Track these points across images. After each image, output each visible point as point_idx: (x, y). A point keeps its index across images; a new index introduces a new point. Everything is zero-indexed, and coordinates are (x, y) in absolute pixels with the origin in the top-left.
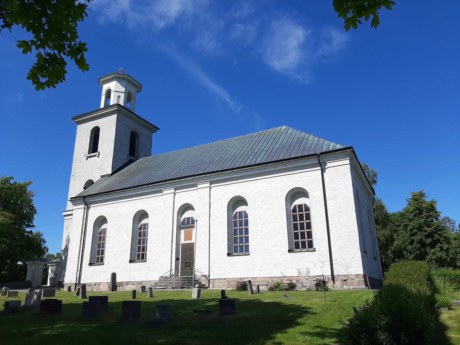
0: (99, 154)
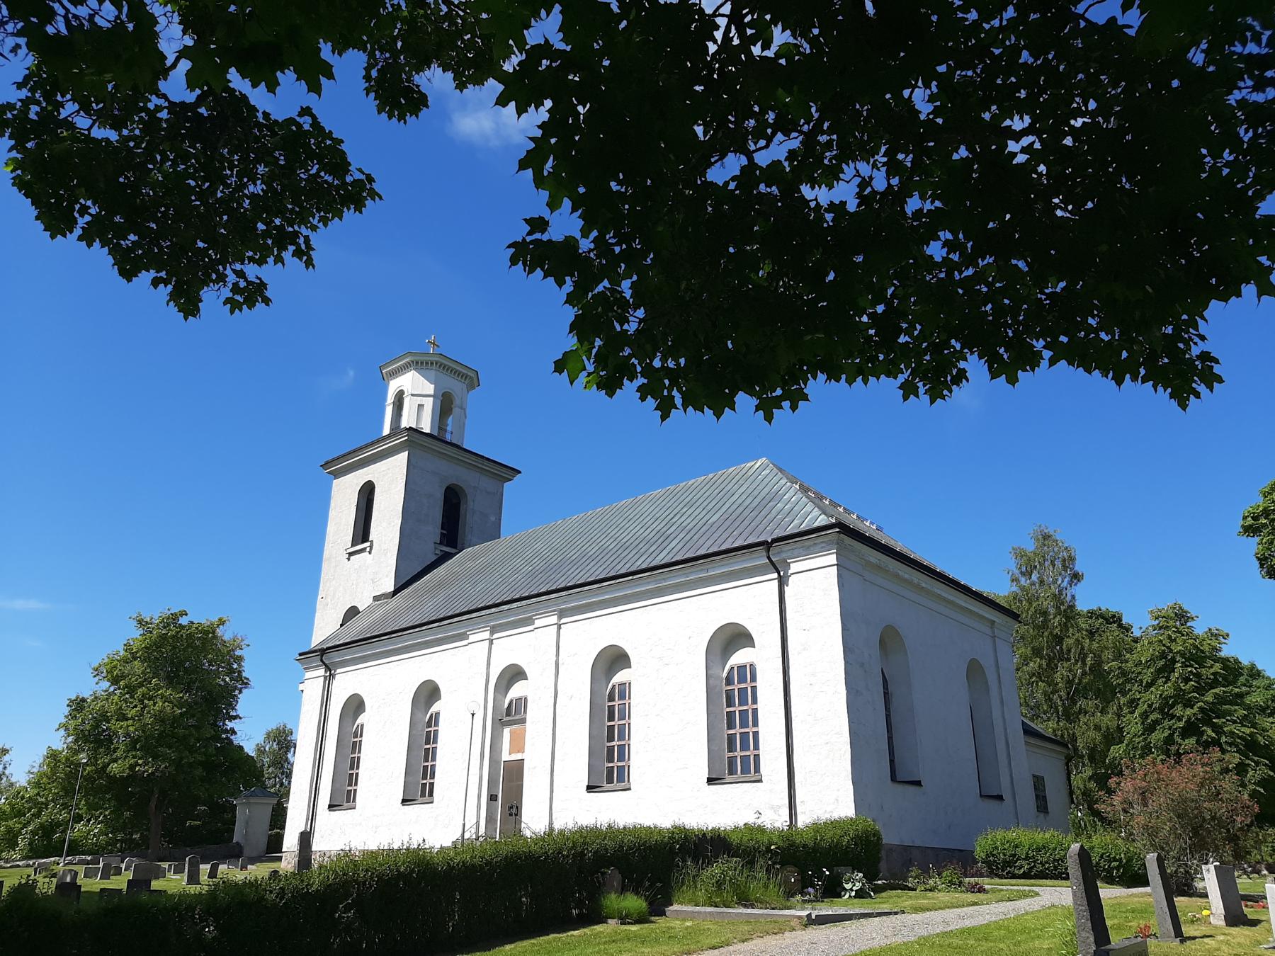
0: (371, 547)
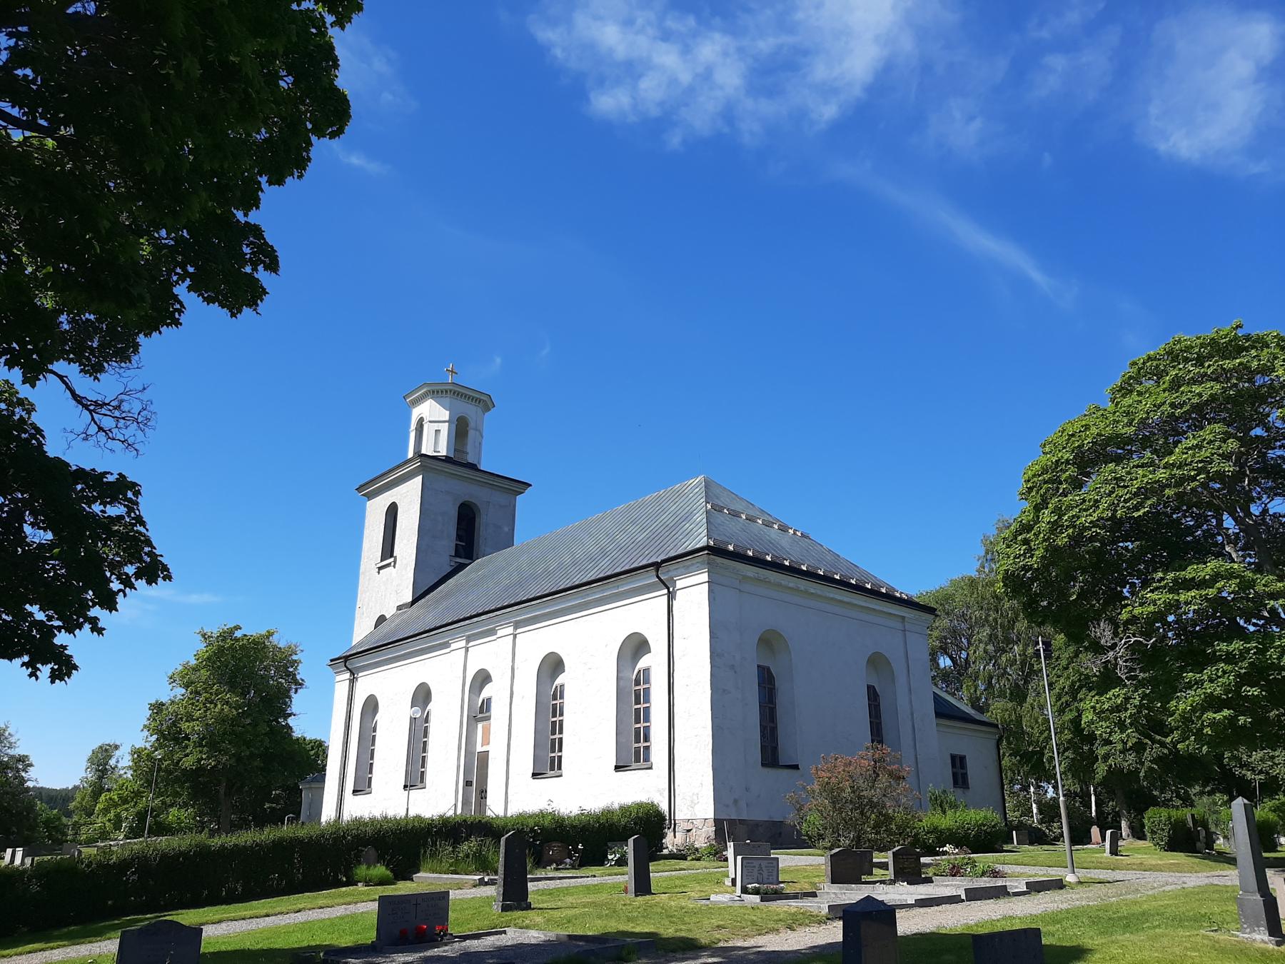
0: (395, 562)
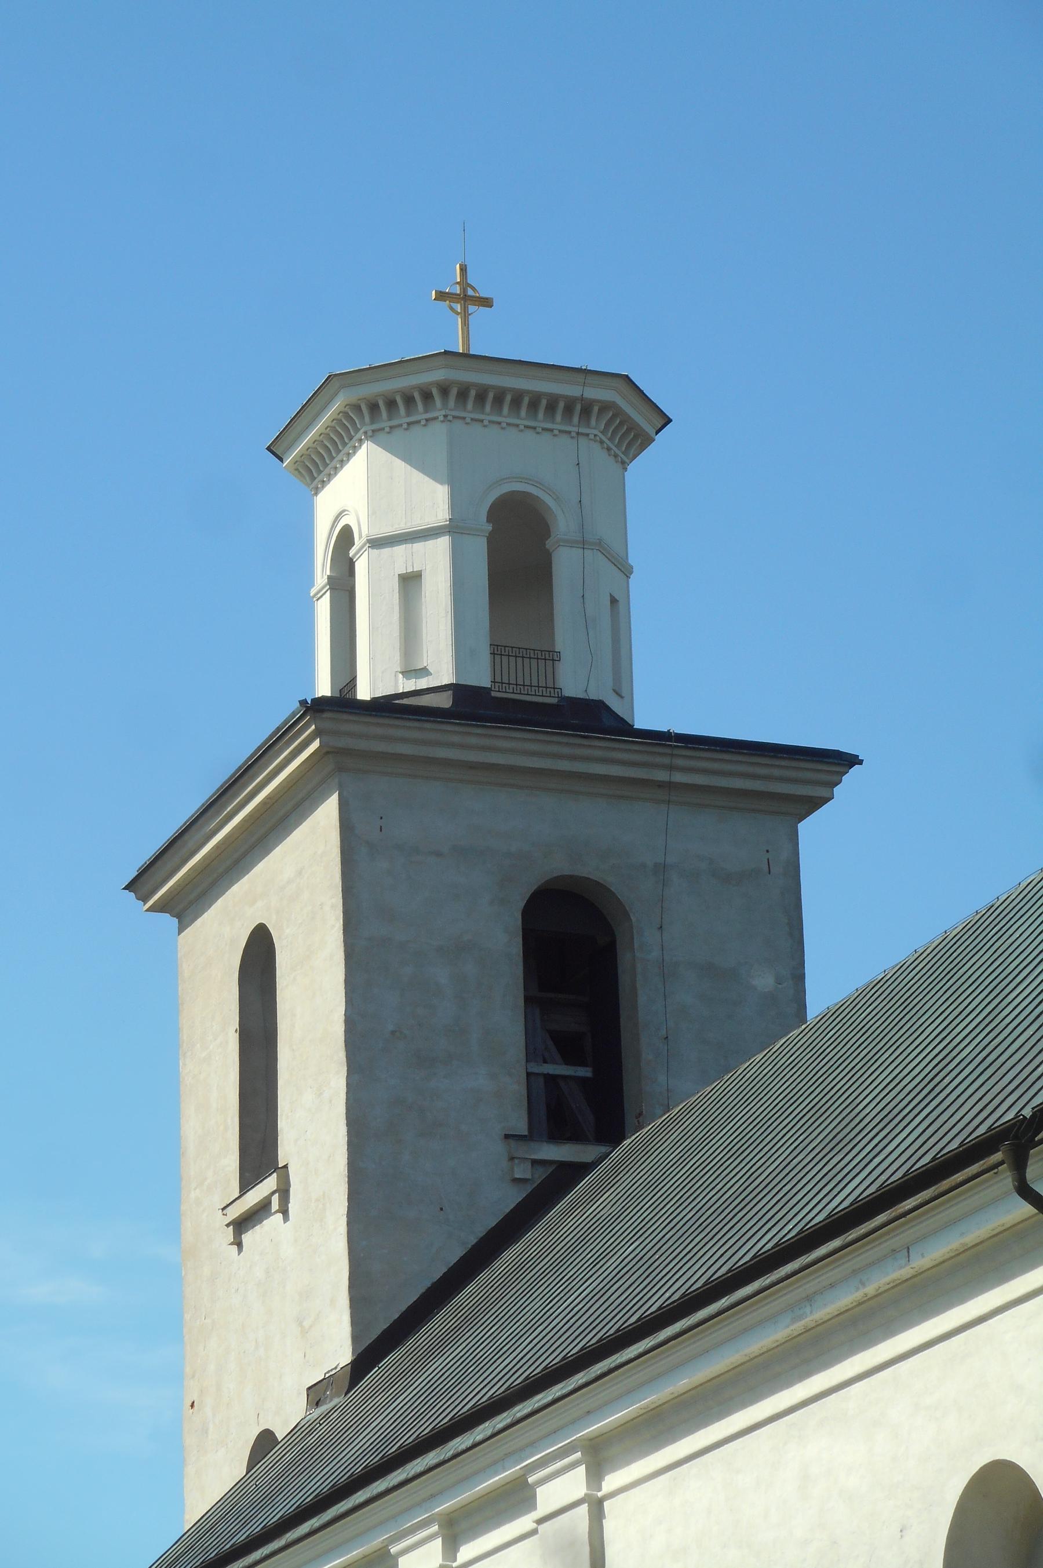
0: (284, 1191)
